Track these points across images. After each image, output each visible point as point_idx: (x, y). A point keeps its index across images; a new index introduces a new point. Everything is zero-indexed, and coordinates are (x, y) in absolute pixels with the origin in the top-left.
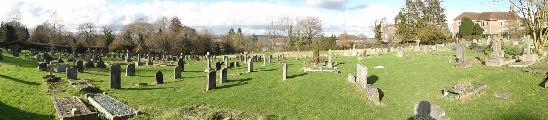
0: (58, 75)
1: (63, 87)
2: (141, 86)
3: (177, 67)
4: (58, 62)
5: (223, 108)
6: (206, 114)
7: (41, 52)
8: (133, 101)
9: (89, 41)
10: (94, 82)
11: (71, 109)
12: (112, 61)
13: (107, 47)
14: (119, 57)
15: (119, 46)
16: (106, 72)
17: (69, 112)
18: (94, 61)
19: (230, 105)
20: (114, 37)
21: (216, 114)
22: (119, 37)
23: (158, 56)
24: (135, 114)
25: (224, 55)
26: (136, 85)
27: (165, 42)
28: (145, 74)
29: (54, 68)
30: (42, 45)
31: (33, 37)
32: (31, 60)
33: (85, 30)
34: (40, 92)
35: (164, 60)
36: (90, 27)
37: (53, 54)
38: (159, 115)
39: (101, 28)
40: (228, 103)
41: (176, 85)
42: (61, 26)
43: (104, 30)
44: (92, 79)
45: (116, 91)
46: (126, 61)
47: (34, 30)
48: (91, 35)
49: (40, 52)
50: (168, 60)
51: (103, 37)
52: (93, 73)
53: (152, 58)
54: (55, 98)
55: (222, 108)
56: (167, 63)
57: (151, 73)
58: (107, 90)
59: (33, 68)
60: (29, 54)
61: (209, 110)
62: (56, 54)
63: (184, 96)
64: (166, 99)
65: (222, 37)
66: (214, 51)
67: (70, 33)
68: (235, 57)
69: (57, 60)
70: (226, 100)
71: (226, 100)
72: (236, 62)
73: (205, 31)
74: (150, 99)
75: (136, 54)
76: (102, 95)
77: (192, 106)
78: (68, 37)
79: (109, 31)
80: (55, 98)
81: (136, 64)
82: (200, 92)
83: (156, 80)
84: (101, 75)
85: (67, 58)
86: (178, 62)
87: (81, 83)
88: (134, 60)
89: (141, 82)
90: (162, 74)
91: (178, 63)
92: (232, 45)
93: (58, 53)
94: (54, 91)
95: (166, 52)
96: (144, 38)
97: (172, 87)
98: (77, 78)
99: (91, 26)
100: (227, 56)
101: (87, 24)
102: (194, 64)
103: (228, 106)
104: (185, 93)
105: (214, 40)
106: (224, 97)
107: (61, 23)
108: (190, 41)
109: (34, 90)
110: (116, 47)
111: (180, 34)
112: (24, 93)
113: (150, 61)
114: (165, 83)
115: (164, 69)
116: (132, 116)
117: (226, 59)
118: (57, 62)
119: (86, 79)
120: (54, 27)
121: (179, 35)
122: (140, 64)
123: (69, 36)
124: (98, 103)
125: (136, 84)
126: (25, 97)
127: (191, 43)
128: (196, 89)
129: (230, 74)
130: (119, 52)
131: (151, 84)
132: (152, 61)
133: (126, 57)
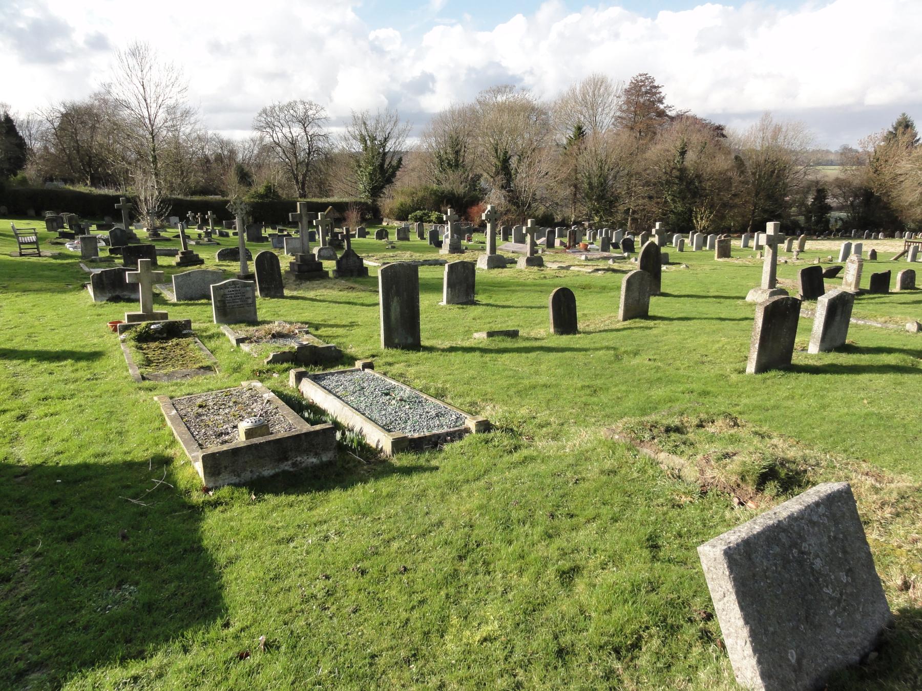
0: (177, 315)
1: (198, 354)
2: (496, 338)
3: (632, 276)
4: (179, 265)
5: (815, 447)
6: (734, 454)
7: (100, 227)
8: (462, 389)
9: (305, 176)
10: (323, 329)
11: (235, 427)
12: (391, 254)
13: (374, 201)
14: (421, 236)
15: (420, 194)
16: (371, 291)
17: (227, 437)
18: (324, 253)
19: (849, 443)
20: (400, 160)
21: (782, 464)
22: (418, 162)
23: (564, 232)
24: (467, 431)
25: (843, 237)
26: (476, 335)
27: (595, 181)
28: (513, 299)
29: (157, 289)
30: (100, 195)
31: (46, 156)
32: (54, 261)
33: (286, 130)
34: (102, 386)
35: (587, 250)
36: (304, 122)
37: (155, 233)
38: (553, 439)
39: (346, 124)
40: (838, 432)
41: (625, 341)
42: (178, 114)
43: (357, 132)
44: (318, 320)
45: (403, 358)
46: (444, 251)
47: (48, 125)
48: (309, 154)
49: (94, 227)
50: (605, 248)
51: (358, 161)
52: (322, 298)
53: (543, 239)
54: (171, 398)
55: (810, 446)
56: (598, 259)
57: (536, 295)
58: (370, 353)
59: (64, 296)
60: (36, 234)
61: (750, 444)
62: (168, 233)
63: (651, 382)
64: (583, 387)
65: (848, 157)
66: (801, 219)
67: (223, 144)
68: (902, 249)
69: (172, 254)
70: (832, 422)
71: (832, 422)
72: (904, 274)
73: (769, 134)
74: (526, 382)
75: (482, 227)
76: (352, 371)
77: (681, 421)
78: (216, 160)
79: (379, 138)
80: (171, 398)
81: (482, 264)
82: (716, 376)
83: (551, 321)
84: (349, 303)
85: (218, 244)
86: (639, 259)
87: (274, 336)
88: (474, 249)
89: (497, 327)
90: (574, 301)
91: (638, 263)
92: (894, 194)
93: (175, 226)
94: (165, 375)
95: (597, 219)
96: (513, 162)
97: (608, 348)
98: (259, 319)
99: (306, 116)
100: (859, 242)
101: (291, 106)
102: (707, 268)
103: (835, 444)
104: (657, 372)
105: (805, 174)
106: (824, 407)
107: (172, 97)
108: (698, 176)
109: (76, 381)
110: (408, 201)
111: (659, 147)
112: (28, 398)
113: (533, 251)
114: (584, 333)
115: (585, 283)
116: (459, 434)
117: (853, 257)
118: (174, 263)
119: (294, 319)
120: (146, 115)
121: (654, 152)
122: (497, 262)
123: (219, 158)
124: (338, 397)
125: (476, 331)
126: (37, 412)
127: (700, 182)
128: (703, 363)
129: (861, 322)
130: (421, 220)
131: (533, 334)
132: (543, 251)
133: (446, 234)
